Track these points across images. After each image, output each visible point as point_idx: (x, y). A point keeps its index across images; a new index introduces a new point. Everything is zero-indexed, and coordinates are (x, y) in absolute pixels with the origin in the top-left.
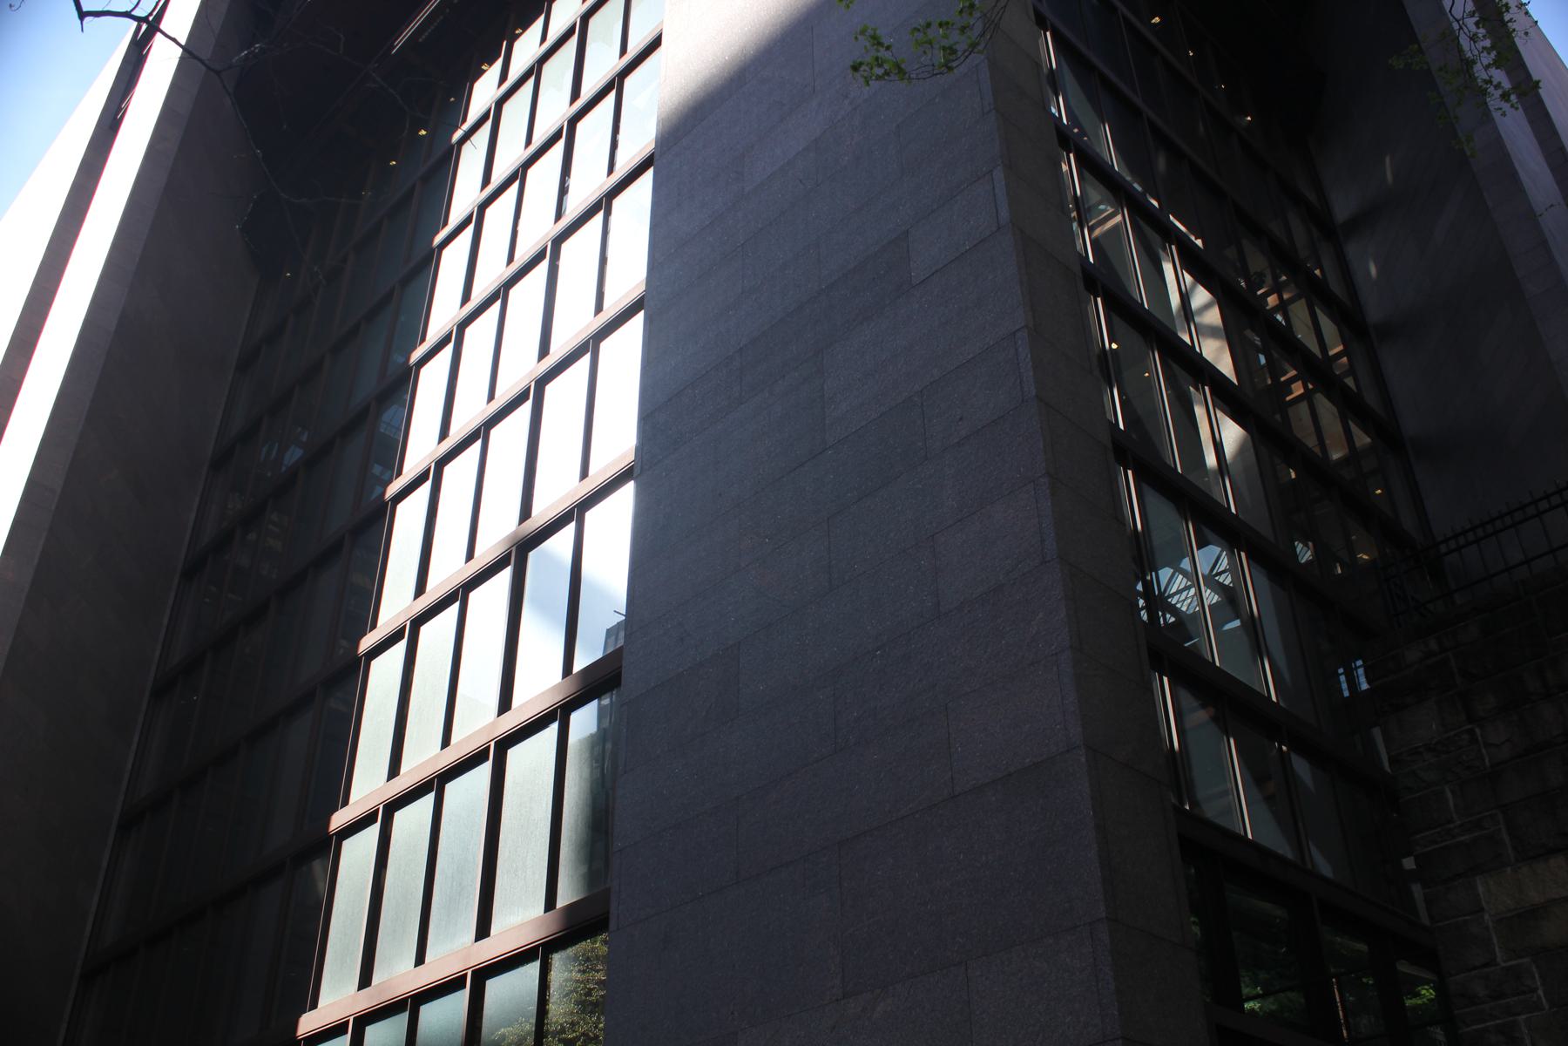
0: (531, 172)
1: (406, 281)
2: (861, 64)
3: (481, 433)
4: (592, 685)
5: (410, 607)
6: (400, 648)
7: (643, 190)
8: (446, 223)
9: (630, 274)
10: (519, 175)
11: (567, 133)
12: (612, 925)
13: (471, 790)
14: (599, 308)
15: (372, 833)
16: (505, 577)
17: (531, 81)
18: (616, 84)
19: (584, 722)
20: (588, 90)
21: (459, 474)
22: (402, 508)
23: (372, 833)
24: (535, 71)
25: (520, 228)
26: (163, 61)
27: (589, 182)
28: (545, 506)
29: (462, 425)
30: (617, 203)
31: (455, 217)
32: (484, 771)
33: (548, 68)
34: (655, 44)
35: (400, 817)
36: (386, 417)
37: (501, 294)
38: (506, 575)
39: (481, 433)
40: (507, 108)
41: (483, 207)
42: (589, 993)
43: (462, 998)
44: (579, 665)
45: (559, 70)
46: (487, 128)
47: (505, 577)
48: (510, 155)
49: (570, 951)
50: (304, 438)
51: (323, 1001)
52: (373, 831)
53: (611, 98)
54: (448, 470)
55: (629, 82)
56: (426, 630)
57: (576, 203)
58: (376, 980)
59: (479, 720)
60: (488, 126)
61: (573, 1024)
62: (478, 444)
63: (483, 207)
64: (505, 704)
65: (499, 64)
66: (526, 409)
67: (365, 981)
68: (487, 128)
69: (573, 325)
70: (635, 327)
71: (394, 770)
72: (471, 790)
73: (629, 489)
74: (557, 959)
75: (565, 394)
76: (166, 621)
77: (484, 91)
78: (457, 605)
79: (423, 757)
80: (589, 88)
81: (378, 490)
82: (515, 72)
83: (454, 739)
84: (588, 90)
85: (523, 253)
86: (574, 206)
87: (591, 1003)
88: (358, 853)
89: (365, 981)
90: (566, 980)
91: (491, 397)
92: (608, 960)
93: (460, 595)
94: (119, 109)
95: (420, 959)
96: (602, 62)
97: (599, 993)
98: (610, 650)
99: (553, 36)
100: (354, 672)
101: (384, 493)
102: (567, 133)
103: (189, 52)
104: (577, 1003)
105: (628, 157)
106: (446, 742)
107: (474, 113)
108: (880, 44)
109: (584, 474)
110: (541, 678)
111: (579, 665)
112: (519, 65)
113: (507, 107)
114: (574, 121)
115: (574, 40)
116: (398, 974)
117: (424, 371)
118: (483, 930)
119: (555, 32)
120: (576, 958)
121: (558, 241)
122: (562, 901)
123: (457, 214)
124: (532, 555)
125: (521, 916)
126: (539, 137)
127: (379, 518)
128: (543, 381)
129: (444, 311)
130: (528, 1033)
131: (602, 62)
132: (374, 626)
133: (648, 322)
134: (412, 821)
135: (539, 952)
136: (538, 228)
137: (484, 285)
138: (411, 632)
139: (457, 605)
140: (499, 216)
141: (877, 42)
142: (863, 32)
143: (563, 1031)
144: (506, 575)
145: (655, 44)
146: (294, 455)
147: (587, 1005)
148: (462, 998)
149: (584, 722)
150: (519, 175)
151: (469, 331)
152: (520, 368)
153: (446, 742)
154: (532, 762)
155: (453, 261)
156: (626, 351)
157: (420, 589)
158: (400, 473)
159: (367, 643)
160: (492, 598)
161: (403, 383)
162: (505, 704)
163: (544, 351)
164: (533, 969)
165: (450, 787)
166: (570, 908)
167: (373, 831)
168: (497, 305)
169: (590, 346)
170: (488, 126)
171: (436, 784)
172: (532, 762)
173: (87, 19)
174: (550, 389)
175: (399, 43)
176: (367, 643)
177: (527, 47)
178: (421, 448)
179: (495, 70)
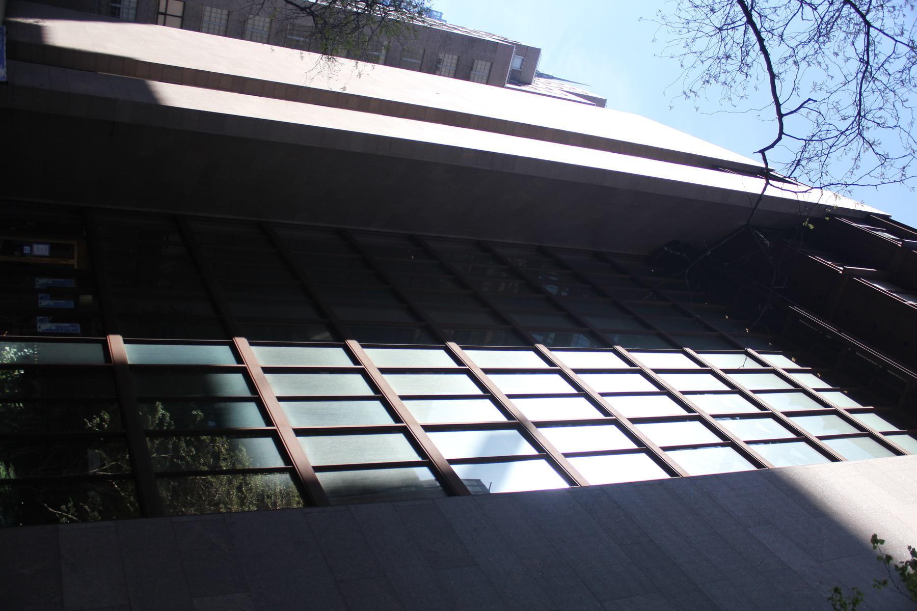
0: (737, 397)
2: (840, 593)
4: (445, 478)
6: (453, 365)
8: (698, 352)
9: (692, 465)
10: (735, 390)
11: (765, 413)
12: (306, 510)
13: (378, 415)
14: (665, 449)
16: (501, 418)
18: (800, 437)
19: (424, 475)
20: (793, 421)
21: (556, 384)
24: (798, 388)
26: (753, 185)
27: (738, 430)
28: (546, 436)
29: (585, 380)
30: (729, 450)
32: (389, 422)
33: (801, 395)
34: (833, 458)
35: (359, 377)
36: (582, 336)
38: (502, 419)
40: (772, 376)
41: (712, 372)
42: (269, 497)
43: (260, 425)
44: (456, 468)
45: (801, 402)
46: (758, 366)
47: (501, 418)
49: (291, 483)
50: (564, 294)
53: (791, 436)
54: (557, 377)
55: (803, 445)
57: (725, 426)
58: (268, 376)
59: (417, 415)
60: (759, 367)
61: (251, 489)
63: (712, 372)
65: (797, 367)
66: (599, 416)
67: (267, 370)
68: (758, 366)
71: (384, 371)
72: (378, 415)
73: (564, 485)
74: (286, 477)
75: (612, 437)
76: (451, 236)
77: (779, 361)
78: (481, 393)
79: (393, 386)
80: (731, 378)
82: (794, 377)
83: (405, 402)
84: (793, 421)
85: (689, 400)
86: (722, 424)
88: (336, 357)
90: (275, 483)
91: (603, 395)
92: (287, 509)
93: (487, 394)
94: (724, 168)
95: (280, 399)
96: (812, 426)
98: (465, 483)
100: (436, 341)
102: (765, 413)
103: (761, 198)
104: (263, 491)
105: (757, 451)
106: (403, 398)
107: (765, 358)
108: (854, 605)
109: (567, 455)
110: (445, 447)
111: (456, 468)
112: (798, 378)
113: (772, 376)
114: (773, 416)
115: (821, 408)
116: (272, 388)
118: (299, 432)
119: (823, 396)
120: (288, 487)
122: (319, 476)
124: (515, 432)
125: (309, 453)
126: (759, 397)
127: (524, 342)
128: (617, 423)
129: (648, 360)
130: (244, 465)
131: (812, 426)
132: (463, 348)
135: (290, 467)
136: (706, 406)
138: (463, 369)
139: (481, 393)
141: (855, 602)
142: (858, 593)
143: (247, 484)
144: (502, 419)
145: (833, 458)
146: (552, 290)
147: (261, 497)
148: (260, 425)
149: (424, 475)
150: (735, 390)
151: (639, 376)
153: (403, 398)
154: (398, 448)
155: (677, 360)
156: (643, 470)
157: (487, 371)
158: (551, 350)
159: (453, 346)
160: (487, 412)
161: (602, 344)
162: (428, 428)
163: (635, 421)
164: (280, 464)
166: (316, 482)
169: (642, 447)
171: (379, 396)
172: (398, 448)
173: (760, 155)
175: (796, 309)
176: (453, 346)
177: (810, 381)
178: (568, 359)
179: (793, 365)
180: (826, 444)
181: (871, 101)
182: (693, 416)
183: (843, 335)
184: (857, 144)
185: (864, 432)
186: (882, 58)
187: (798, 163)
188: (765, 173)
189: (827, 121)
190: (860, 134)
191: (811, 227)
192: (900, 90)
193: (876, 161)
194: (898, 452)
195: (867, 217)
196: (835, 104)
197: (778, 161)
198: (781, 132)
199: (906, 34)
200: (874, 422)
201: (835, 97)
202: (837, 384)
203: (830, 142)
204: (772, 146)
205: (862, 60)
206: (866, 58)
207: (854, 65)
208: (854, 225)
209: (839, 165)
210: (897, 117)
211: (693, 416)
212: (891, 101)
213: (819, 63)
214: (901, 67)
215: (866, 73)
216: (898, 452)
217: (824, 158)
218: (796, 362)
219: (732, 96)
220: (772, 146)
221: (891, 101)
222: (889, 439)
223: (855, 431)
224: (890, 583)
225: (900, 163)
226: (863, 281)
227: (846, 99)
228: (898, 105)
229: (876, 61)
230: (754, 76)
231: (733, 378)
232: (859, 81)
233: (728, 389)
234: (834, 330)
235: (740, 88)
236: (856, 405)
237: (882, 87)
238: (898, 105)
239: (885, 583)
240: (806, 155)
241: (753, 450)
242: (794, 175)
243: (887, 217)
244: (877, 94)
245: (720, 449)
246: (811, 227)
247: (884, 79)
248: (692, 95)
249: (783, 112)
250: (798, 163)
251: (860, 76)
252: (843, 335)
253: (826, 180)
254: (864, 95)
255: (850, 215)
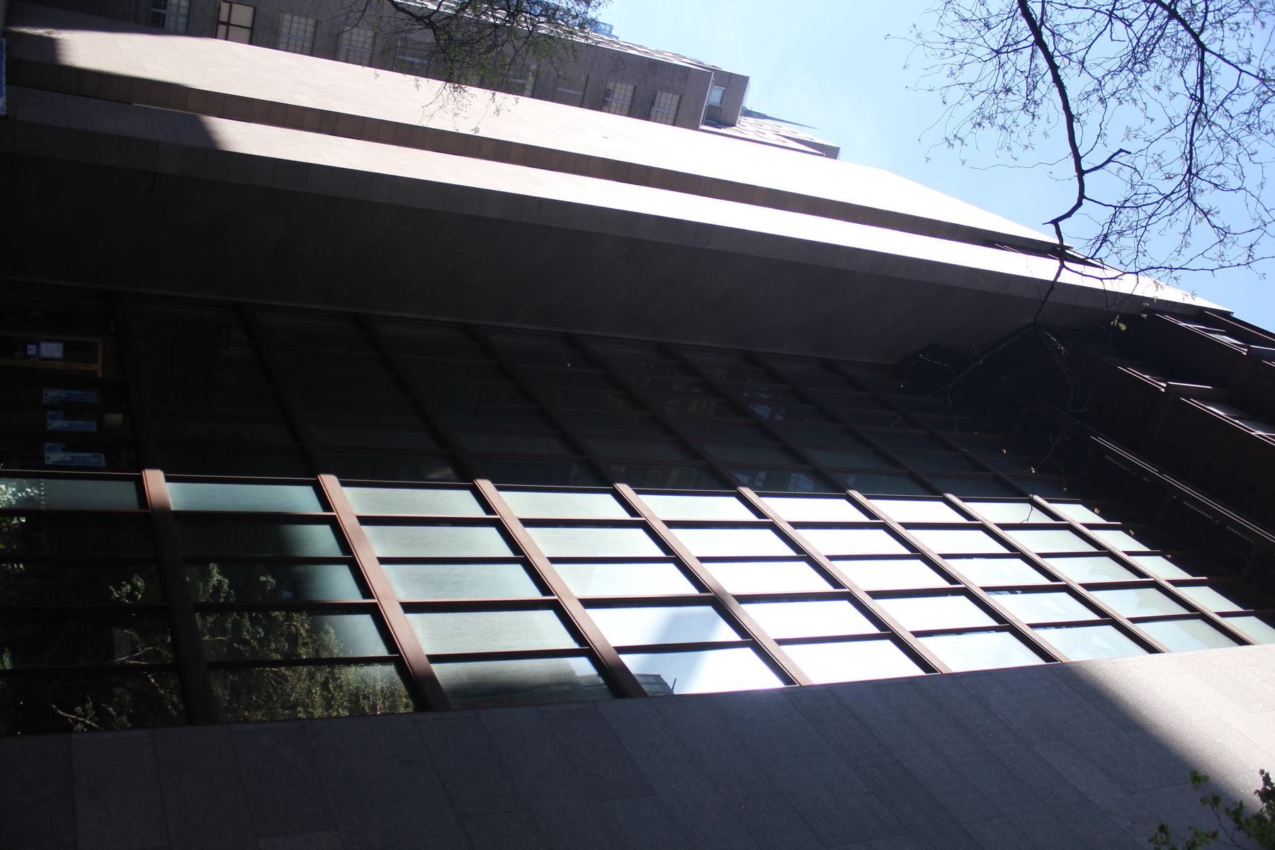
0: (1018, 562)
1: (912, 477)
3: (802, 555)
4: (612, 674)
5: (656, 518)
6: (623, 515)
7: (1026, 658)
8: (964, 500)
9: (954, 657)
11: (1057, 586)
13: (518, 585)
14: (918, 634)
15: (478, 512)
16: (690, 590)
17: (1093, 549)
18: (1105, 618)
19: (582, 667)
20: (1095, 596)
21: (767, 542)
22: (733, 501)
23: (478, 512)
24: (1102, 551)
25: (975, 560)
26: (1042, 269)
27: (1019, 609)
28: (752, 615)
29: (807, 538)
31: (971, 507)
32: (534, 593)
35: (492, 532)
36: (803, 477)
37: (916, 553)
38: (691, 590)
39: (802, 555)
42: (366, 697)
43: (355, 596)
44: (627, 659)
45: (1106, 571)
47: (690, 590)
48: (1029, 542)
49: (397, 678)
50: (779, 417)
51: (347, 491)
52: (479, 513)
53: (1093, 617)
55: (1109, 629)
56: (640, 533)
57: (1001, 602)
58: (365, 528)
59: (573, 584)
62: (792, 553)
64: (589, 603)
66: (827, 587)
67: (364, 520)
69: (902, 615)
70: (1030, 659)
71: (528, 523)
72: (518, 585)
73: (776, 683)
74: (390, 669)
75: (845, 618)
77: (1076, 513)
78: (877, 631)
79: (540, 544)
81: (745, 479)
82: (1097, 535)
84: (1095, 596)
85: (952, 566)
87: (358, 700)
88: (461, 503)
89: (364, 520)
90: (374, 678)
91: (831, 558)
92: (391, 715)
93: (671, 556)
94: (1002, 244)
95: (383, 561)
96: (1121, 604)
97: (366, 705)
98: (639, 680)
99: (1134, 560)
100: (600, 481)
101: (744, 485)
102: (1057, 586)
104: (357, 689)
105: (1046, 638)
106: (554, 560)
107: (1057, 508)
110: (612, 629)
111: (627, 659)
112: (1103, 537)
113: (1067, 533)
116: (371, 545)
117: (844, 502)
118: (409, 607)
119: (1137, 561)
121: (967, 593)
123: (975, 508)
125: (422, 637)
126: (1049, 563)
127: (722, 484)
129: (895, 510)
130: (331, 652)
131: (1121, 604)
132: (638, 492)
133: (911, 681)
134: (489, 542)
135: (395, 656)
136: (975, 574)
137: (921, 538)
138: (637, 521)
140: (979, 541)
143: (335, 679)
144: (691, 590)
145: (1151, 649)
146: (763, 411)
147: (356, 698)
148: (355, 596)
149: (582, 667)
150: (1015, 552)
152: (859, 577)
154: (545, 630)
155: (935, 511)
156: (887, 663)
157: (671, 524)
158: (760, 495)
159: (625, 489)
160: (671, 582)
161: (831, 487)
162: (589, 603)
163: (876, 595)
164: (382, 651)
165: (518, 569)
166: (432, 678)
167: (479, 513)
168: (906, 552)
169: (886, 632)
170: (1048, 520)
171: (520, 557)
172: (545, 630)
173: (1052, 227)
174: (846, 604)
175: (1100, 440)
176: (625, 489)
177: (1119, 541)
178: (783, 508)
179: (1096, 519)
180: (1142, 629)
181: (1206, 153)
182: (956, 588)
183: (1166, 478)
184: (1187, 213)
185: (1194, 613)
186: (1221, 94)
187: (1105, 238)
188: (1059, 252)
189: (1145, 180)
190: (1190, 199)
191: (1123, 327)
192: (1246, 139)
193: (1213, 236)
194: (1241, 641)
195: (1199, 314)
196: (1156, 157)
197: (1077, 235)
198: (1082, 196)
199: (1255, 62)
200: (1208, 599)
201: (1155, 148)
202: (1157, 546)
203: (1150, 210)
204: (1069, 215)
205: (1193, 97)
206: (1199, 95)
207: (1183, 104)
208: (1182, 324)
209: (1162, 241)
210: (1242, 177)
211: (956, 588)
212: (1234, 153)
213: (1134, 100)
214: (1247, 107)
215: (1200, 114)
216: (1241, 641)
217: (1140, 232)
218: (1100, 515)
219: (1013, 145)
220: (1069, 215)
221: (1234, 153)
222: (1228, 622)
223: (1182, 611)
224: (1222, 835)
225: (1246, 240)
226: (1194, 403)
227: (1172, 150)
228: (1243, 159)
229: (1213, 98)
230: (1044, 118)
231: (1013, 536)
232: (1190, 126)
233: (1006, 551)
234: (1153, 470)
235: (1024, 135)
236: (1184, 576)
237: (1221, 134)
238: (1243, 159)
239: (1215, 835)
240: (1116, 227)
241: (1040, 636)
242: (1099, 255)
243: (1227, 315)
244: (1214, 143)
245: (994, 635)
246: (1123, 327)
247: (1224, 123)
248: (958, 142)
249: (1085, 167)
250: (1105, 238)
251: (1191, 118)
252: (1166, 478)
253: (1143, 262)
254: (1197, 144)
255: (1175, 310)
